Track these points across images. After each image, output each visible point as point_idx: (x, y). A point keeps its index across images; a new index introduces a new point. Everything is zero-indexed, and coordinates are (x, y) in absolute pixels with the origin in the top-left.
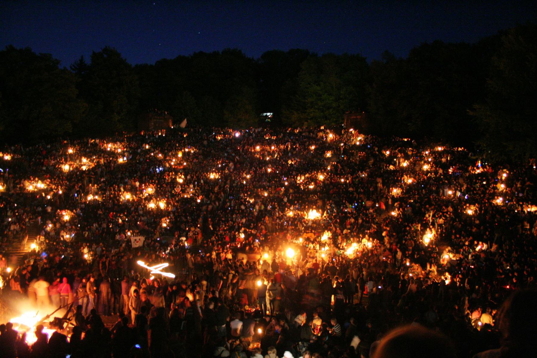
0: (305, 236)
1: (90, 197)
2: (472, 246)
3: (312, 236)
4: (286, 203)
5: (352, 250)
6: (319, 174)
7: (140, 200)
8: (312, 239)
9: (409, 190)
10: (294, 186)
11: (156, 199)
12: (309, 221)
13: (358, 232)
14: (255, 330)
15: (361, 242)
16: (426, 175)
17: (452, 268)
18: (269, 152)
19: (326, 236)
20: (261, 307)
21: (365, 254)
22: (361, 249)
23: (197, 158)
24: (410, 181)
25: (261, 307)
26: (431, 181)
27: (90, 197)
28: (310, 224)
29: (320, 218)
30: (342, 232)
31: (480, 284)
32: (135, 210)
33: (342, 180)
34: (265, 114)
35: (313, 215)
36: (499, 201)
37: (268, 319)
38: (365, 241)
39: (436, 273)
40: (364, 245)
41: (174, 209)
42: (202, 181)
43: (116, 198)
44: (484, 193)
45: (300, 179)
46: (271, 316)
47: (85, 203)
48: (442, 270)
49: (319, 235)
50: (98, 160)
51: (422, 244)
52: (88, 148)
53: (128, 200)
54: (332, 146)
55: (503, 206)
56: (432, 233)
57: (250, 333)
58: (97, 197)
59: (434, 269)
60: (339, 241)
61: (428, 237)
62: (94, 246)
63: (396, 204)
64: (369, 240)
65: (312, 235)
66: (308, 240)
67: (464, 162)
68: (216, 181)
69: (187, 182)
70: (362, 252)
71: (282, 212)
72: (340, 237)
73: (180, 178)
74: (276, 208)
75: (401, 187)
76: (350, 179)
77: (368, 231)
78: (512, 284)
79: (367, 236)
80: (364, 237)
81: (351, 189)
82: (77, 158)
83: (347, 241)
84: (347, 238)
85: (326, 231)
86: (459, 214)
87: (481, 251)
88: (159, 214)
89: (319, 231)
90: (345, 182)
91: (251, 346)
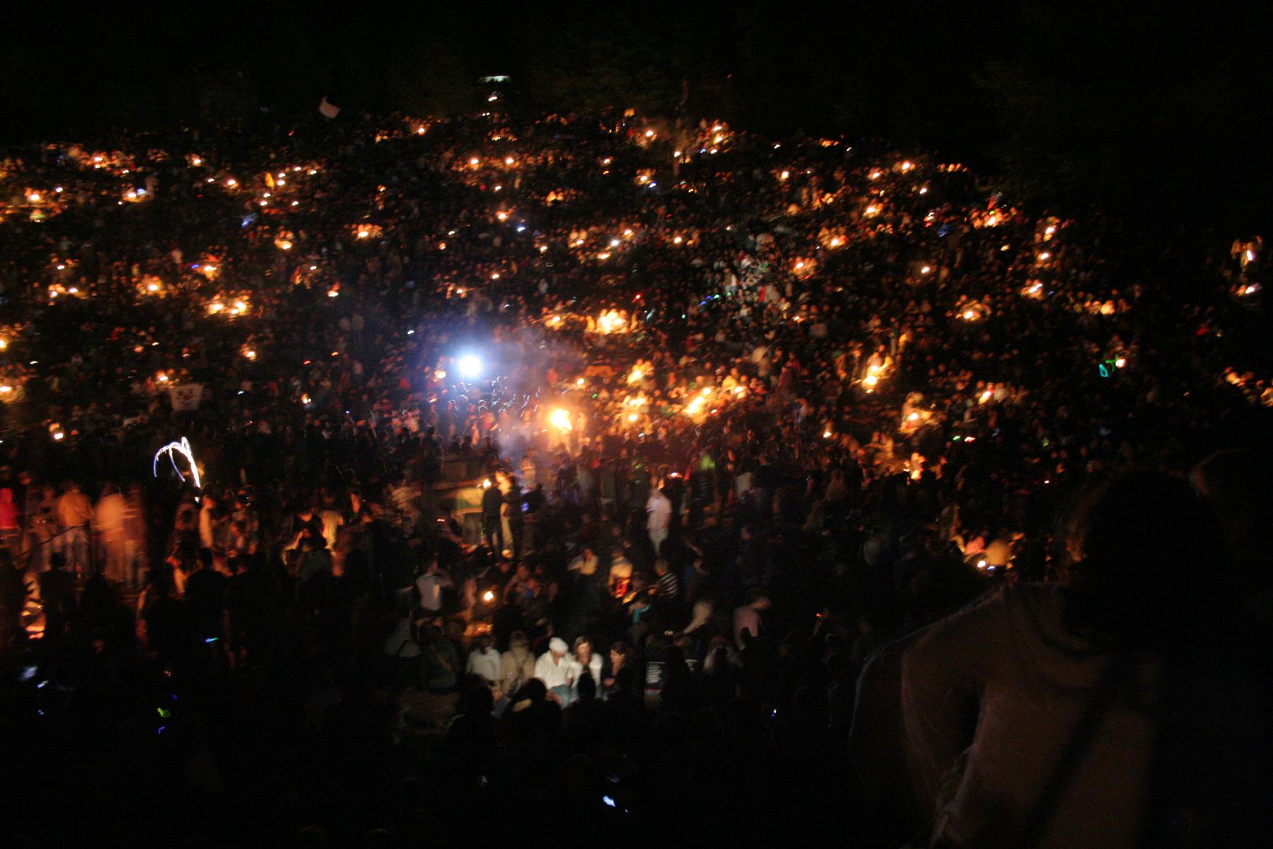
0: (591, 371)
1: (55, 291)
2: (971, 391)
3: (607, 372)
4: (542, 296)
5: (698, 404)
6: (622, 225)
7: (184, 293)
8: (606, 381)
9: (831, 263)
10: (562, 255)
11: (228, 291)
12: (597, 336)
13: (717, 361)
14: (478, 595)
15: (720, 384)
16: (874, 228)
17: (928, 442)
18: (501, 172)
19: (638, 374)
20: (489, 539)
21: (728, 414)
22: (720, 402)
23: (323, 188)
24: (836, 242)
25: (489, 539)
26: (885, 243)
27: (55, 291)
28: (602, 343)
29: (624, 330)
30: (677, 362)
31: (982, 476)
32: (177, 322)
33: (678, 240)
34: (489, 79)
35: (610, 322)
36: (1034, 290)
37: (505, 568)
38: (729, 383)
39: (890, 455)
40: (728, 392)
41: (272, 315)
42: (339, 246)
43: (128, 291)
44: (1002, 271)
45: (578, 239)
46: (515, 561)
47: (44, 305)
48: (905, 447)
49: (625, 368)
50: (70, 196)
51: (862, 390)
52: (40, 164)
53: (156, 296)
54: (656, 157)
55: (1043, 302)
56: (883, 362)
57: (466, 600)
58: (73, 291)
59: (889, 445)
60: (671, 383)
61: (873, 375)
62: (77, 413)
63: (802, 296)
64: (739, 382)
65: (607, 369)
66: (596, 381)
67: (957, 197)
68: (372, 242)
69: (301, 250)
70: (723, 408)
71: (535, 318)
72: (672, 375)
73: (284, 239)
74: (520, 307)
75: (814, 255)
76: (695, 236)
77: (738, 361)
78: (1053, 476)
79: (734, 371)
80: (725, 374)
81: (697, 262)
82: (14, 194)
83: (688, 384)
84: (687, 376)
85: (640, 362)
86: (943, 322)
87: (992, 404)
88: (237, 330)
89: (624, 360)
90: (684, 244)
91: (470, 631)
